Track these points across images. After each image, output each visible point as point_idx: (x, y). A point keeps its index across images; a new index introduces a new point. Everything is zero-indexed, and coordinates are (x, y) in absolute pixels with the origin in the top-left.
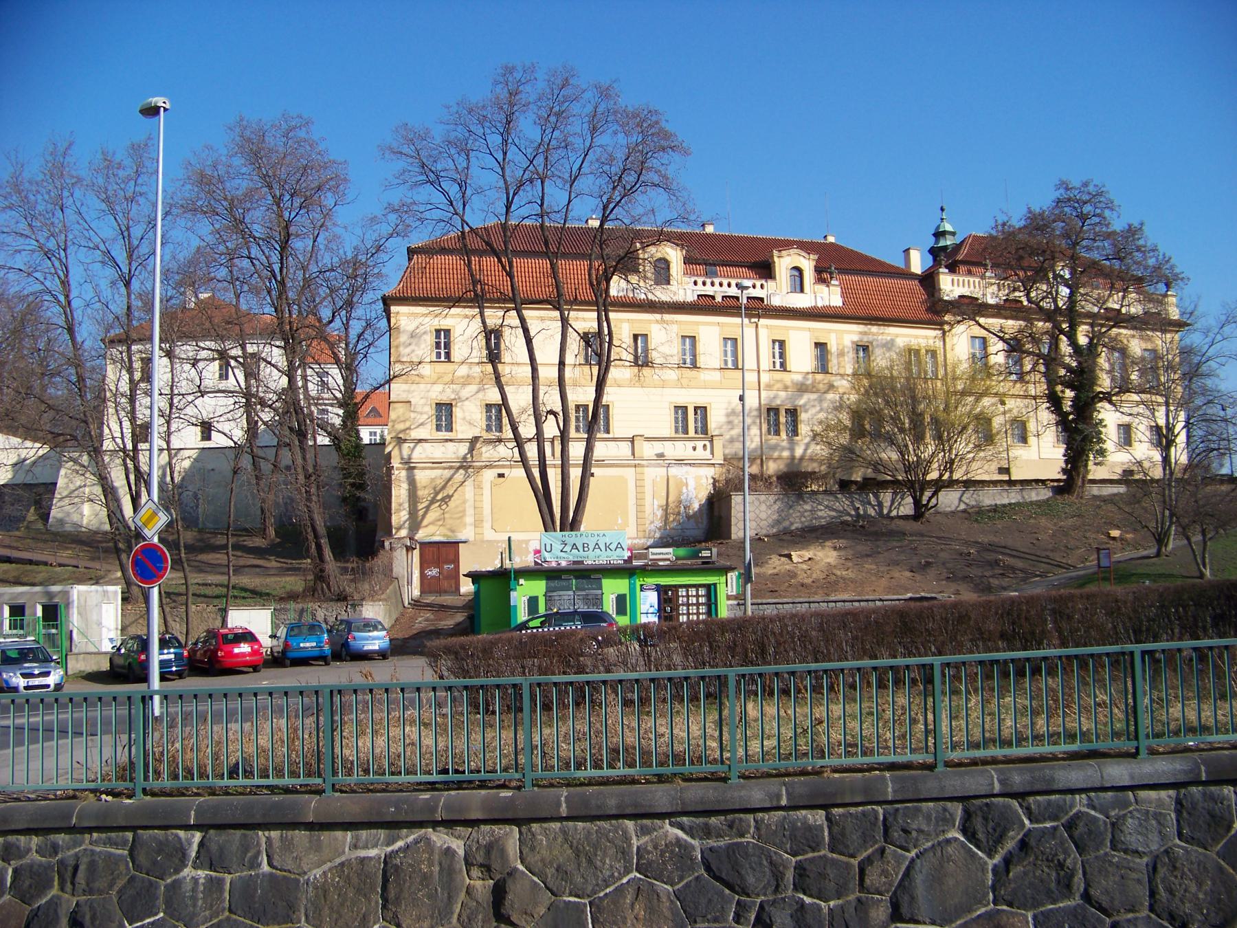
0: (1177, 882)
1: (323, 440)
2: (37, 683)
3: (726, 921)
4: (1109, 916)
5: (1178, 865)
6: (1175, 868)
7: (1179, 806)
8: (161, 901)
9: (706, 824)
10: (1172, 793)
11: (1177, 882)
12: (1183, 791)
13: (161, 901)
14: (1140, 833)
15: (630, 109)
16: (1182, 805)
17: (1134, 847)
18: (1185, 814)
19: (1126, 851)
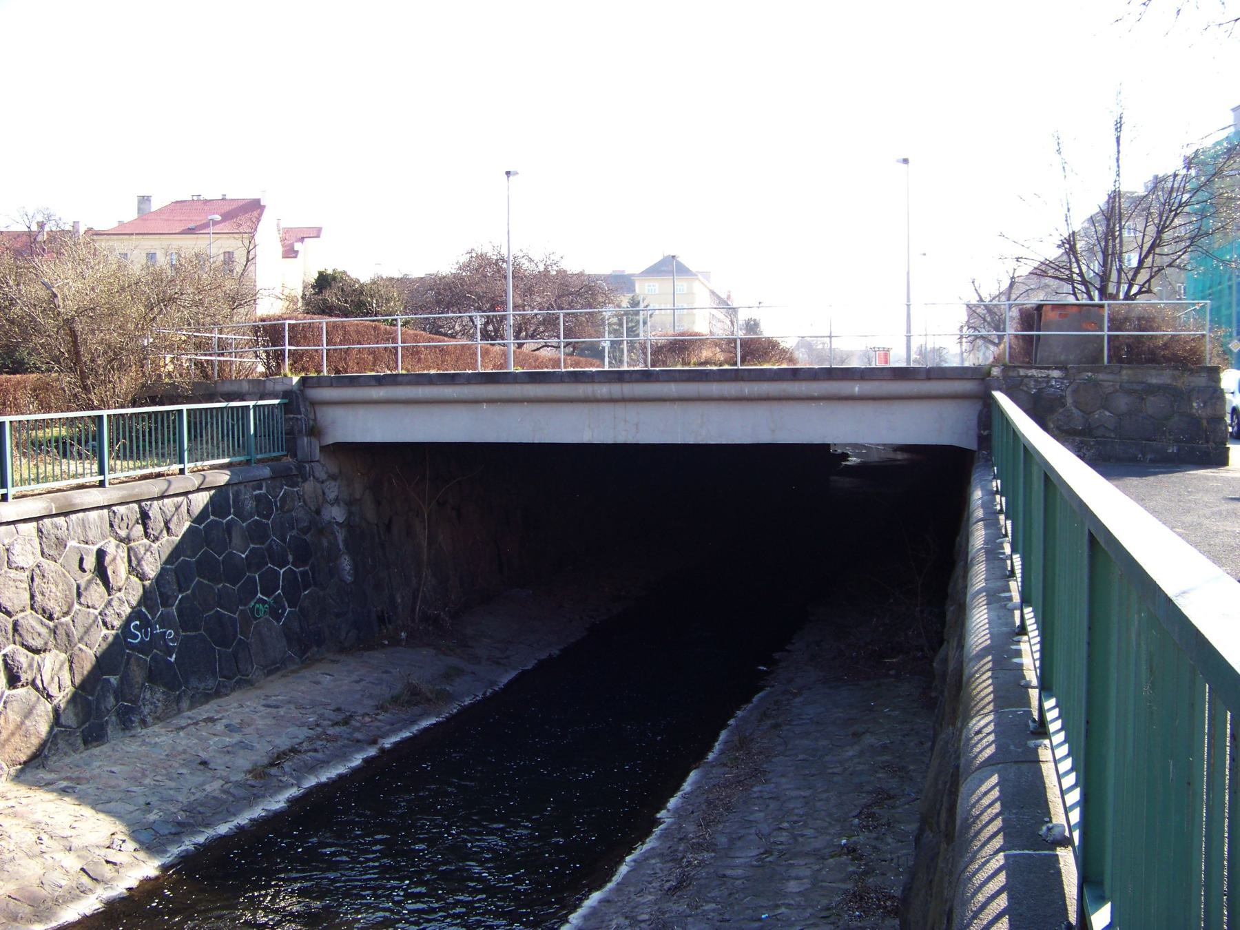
0: (45, 586)
1: (325, 544)
2: (986, 876)
3: (122, 700)
4: (11, 617)
5: (45, 574)
6: (43, 576)
7: (40, 534)
8: (273, 596)
9: (1048, 376)
10: (35, 524)
11: (45, 586)
12: (41, 522)
13: (273, 596)
14: (23, 555)
15: (384, 277)
16: (42, 532)
17: (21, 565)
18: (44, 539)
19: (16, 569)
